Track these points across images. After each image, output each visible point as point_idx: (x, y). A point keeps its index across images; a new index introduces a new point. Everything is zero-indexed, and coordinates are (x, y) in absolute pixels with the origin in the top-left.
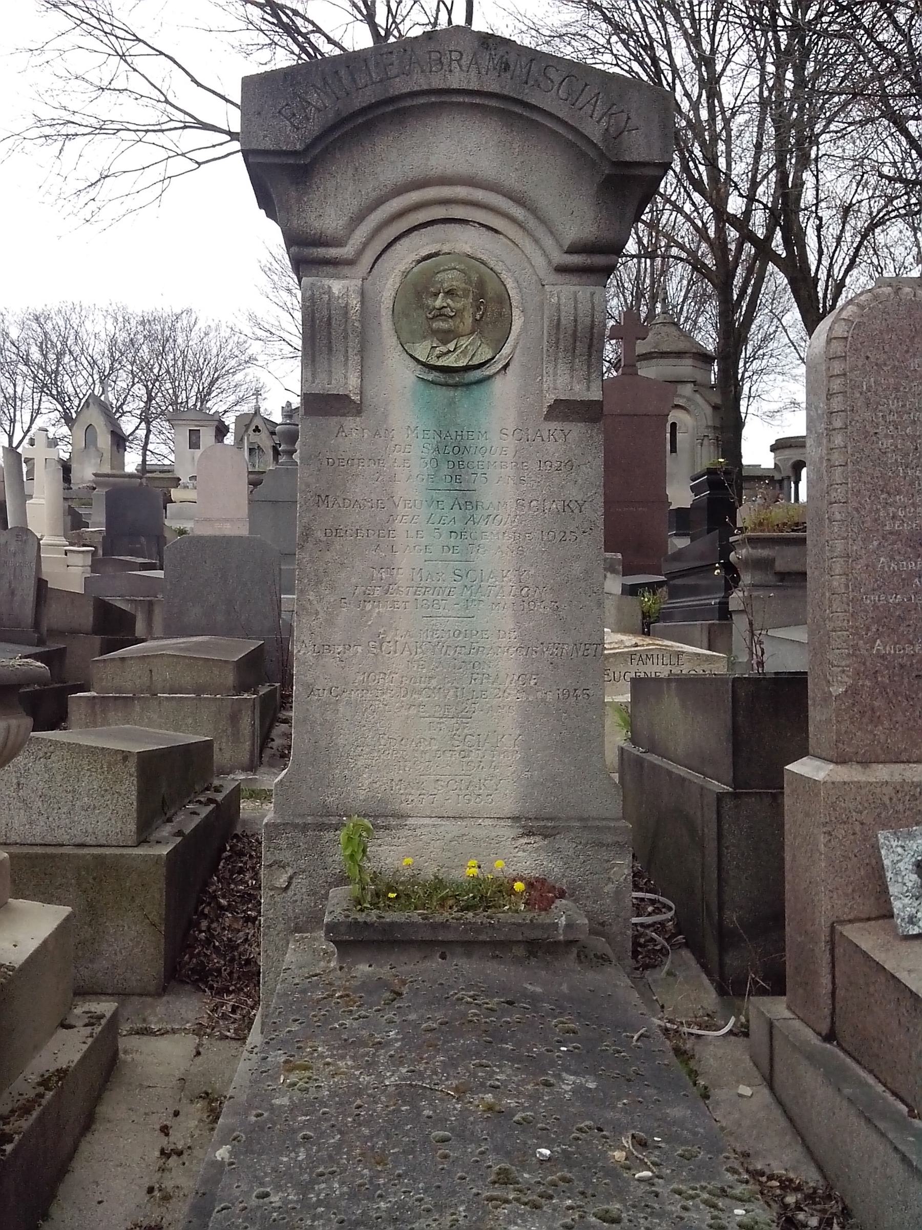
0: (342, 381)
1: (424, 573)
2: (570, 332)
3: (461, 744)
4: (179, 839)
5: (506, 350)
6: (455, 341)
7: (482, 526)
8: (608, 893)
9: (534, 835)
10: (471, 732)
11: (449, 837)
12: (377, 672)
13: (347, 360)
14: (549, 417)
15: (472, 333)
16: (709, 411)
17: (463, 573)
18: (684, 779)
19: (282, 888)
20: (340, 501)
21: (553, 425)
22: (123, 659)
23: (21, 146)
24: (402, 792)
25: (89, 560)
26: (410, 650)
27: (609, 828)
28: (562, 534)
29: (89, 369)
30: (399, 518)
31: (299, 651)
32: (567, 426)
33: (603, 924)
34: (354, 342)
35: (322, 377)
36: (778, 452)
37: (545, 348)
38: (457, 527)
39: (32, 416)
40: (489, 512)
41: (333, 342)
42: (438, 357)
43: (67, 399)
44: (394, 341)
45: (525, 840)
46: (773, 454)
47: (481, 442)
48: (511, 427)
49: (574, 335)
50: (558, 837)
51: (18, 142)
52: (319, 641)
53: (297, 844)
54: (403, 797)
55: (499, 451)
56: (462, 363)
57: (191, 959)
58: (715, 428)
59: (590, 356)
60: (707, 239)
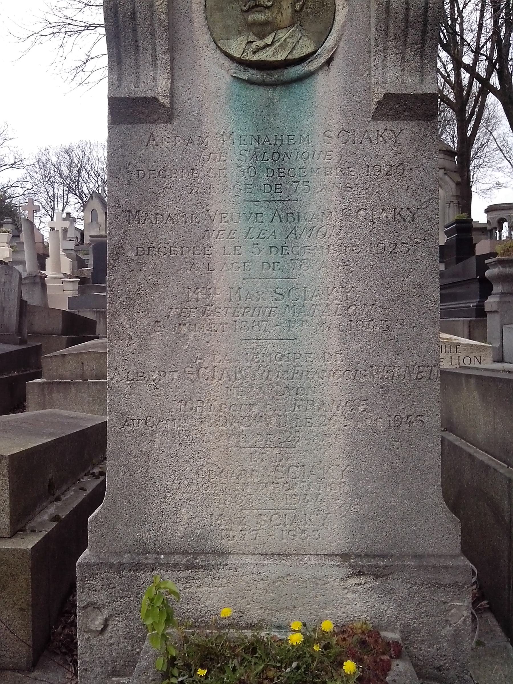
0: (151, 83)
1: (243, 293)
2: (401, 16)
3: (285, 476)
4: (55, 524)
5: (330, 42)
6: (273, 35)
7: (305, 239)
8: (445, 636)
9: (364, 574)
10: (295, 462)
11: (273, 576)
12: (194, 400)
13: (155, 60)
14: (377, 116)
15: (292, 25)
16: (453, 185)
17: (284, 291)
18: (487, 467)
19: (97, 631)
20: (152, 217)
21: (382, 125)
22: (63, 356)
23: (40, 40)
24: (222, 527)
25: (77, 286)
26: (228, 376)
27: (447, 567)
28: (393, 246)
29: (96, 179)
30: (215, 233)
31: (112, 379)
32: (399, 125)
33: (439, 669)
34: (161, 39)
35: (129, 80)
36: (489, 213)
37: (372, 37)
38: (278, 241)
39: (63, 206)
40: (311, 224)
41: (140, 39)
42: (254, 53)
43: (84, 196)
44: (207, 38)
45: (354, 581)
46: (486, 215)
47: (303, 147)
48: (335, 130)
49: (406, 20)
50: (390, 577)
51: (38, 38)
52: (133, 368)
53: (112, 585)
54: (224, 533)
55: (322, 156)
56: (281, 56)
57: (63, 628)
58: (457, 196)
59: (423, 43)
60: (449, 82)
